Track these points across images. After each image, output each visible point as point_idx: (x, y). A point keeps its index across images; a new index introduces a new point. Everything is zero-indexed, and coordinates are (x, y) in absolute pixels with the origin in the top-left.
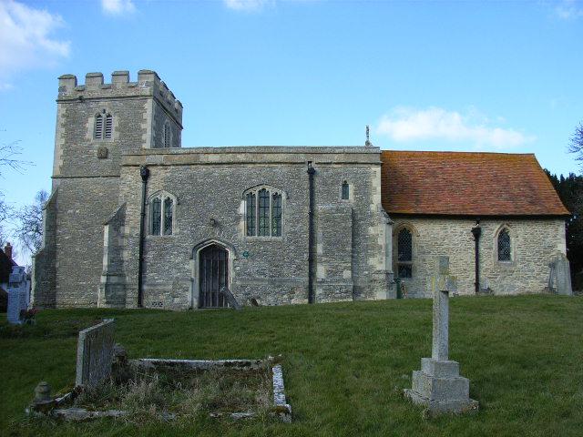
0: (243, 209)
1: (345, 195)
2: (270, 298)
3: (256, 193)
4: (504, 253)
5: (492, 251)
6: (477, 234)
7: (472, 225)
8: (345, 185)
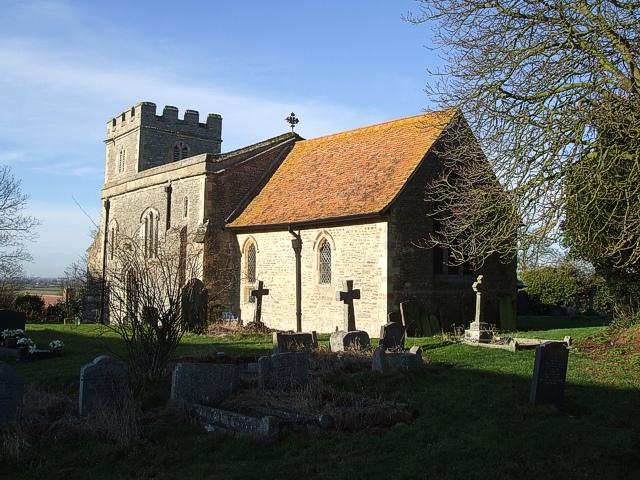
3: (149, 217)
6: (297, 245)
7: (286, 237)
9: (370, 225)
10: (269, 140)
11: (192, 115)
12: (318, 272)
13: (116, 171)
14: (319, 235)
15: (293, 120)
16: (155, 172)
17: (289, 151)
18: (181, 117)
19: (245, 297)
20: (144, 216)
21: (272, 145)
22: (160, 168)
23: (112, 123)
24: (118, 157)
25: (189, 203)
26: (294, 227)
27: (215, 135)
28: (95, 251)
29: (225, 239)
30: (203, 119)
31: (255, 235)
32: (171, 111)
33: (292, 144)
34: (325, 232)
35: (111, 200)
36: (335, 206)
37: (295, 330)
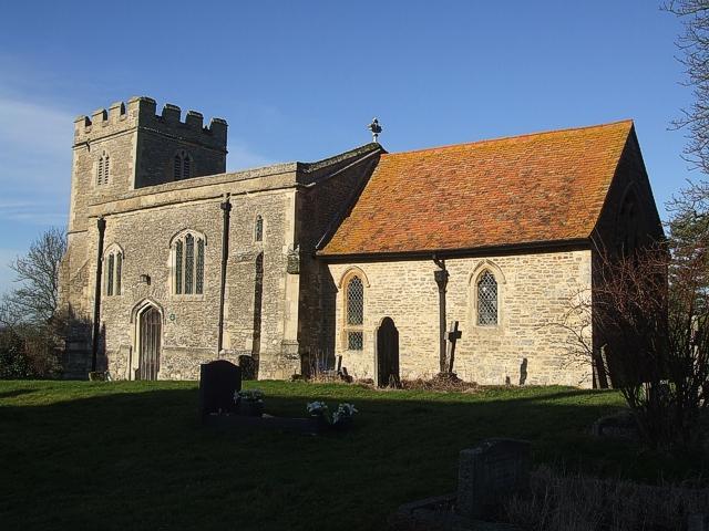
0: (171, 262)
1: (259, 237)
2: (187, 373)
3: (183, 240)
4: (487, 309)
5: (467, 309)
6: (442, 279)
7: (431, 266)
8: (260, 222)
9: (562, 254)
10: (356, 150)
11: (195, 118)
12: (475, 310)
13: (93, 182)
14: (479, 266)
15: (377, 129)
16: (196, 183)
17: (375, 165)
18: (159, 113)
19: (344, 343)
20: (176, 239)
21: (359, 156)
22: (206, 179)
23: (84, 122)
24: (96, 165)
25: (265, 223)
26: (440, 256)
27: (219, 144)
28: (80, 284)
29: (316, 272)
30: (207, 124)
31: (363, 266)
32: (172, 111)
33: (377, 156)
34: (490, 262)
35: (106, 218)
36: (497, 229)
37: (515, 382)
